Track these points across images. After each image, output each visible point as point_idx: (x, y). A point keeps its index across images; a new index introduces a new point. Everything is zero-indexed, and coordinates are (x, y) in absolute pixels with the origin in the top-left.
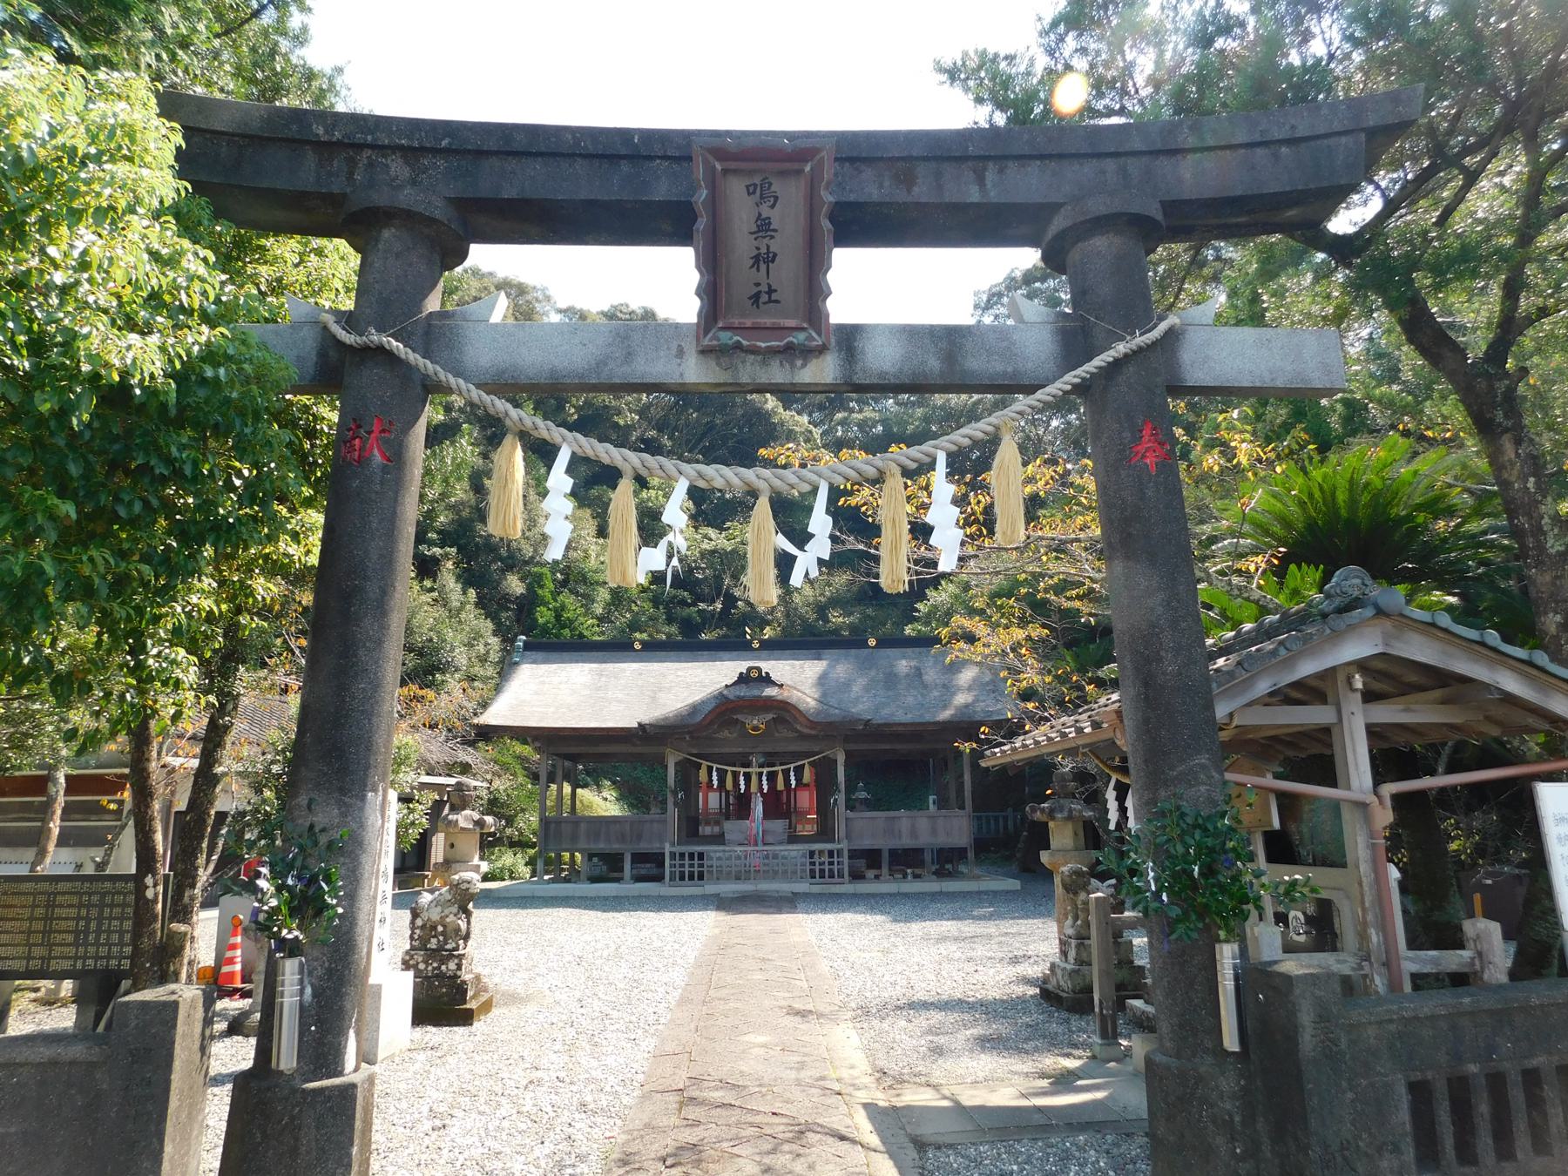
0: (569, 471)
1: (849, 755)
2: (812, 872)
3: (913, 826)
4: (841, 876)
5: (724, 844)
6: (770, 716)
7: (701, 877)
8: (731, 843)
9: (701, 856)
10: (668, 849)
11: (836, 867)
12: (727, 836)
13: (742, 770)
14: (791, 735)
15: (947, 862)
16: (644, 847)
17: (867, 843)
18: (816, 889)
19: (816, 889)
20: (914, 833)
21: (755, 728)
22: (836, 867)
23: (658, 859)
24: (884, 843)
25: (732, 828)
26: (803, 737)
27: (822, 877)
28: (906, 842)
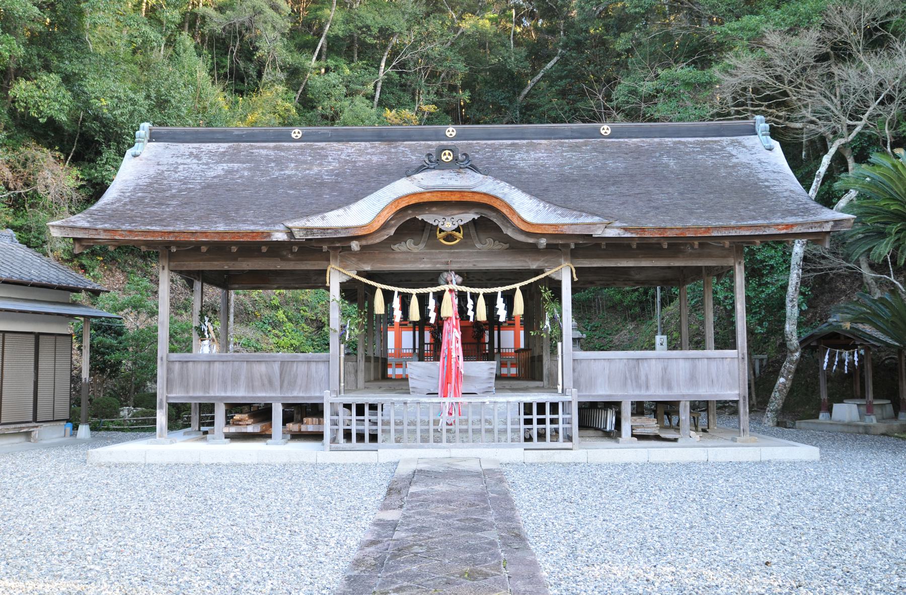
0: (434, 298)
3: (665, 369)
4: (569, 438)
5: (407, 392)
6: (470, 216)
7: (374, 438)
8: (416, 391)
9: (373, 407)
10: (329, 399)
11: (548, 426)
12: (411, 383)
13: (431, 290)
14: (498, 246)
15: (710, 414)
16: (299, 395)
20: (666, 382)
21: (450, 237)
22: (560, 426)
23: (316, 410)
24: (682, 391)
25: (416, 370)
26: (516, 248)
28: (656, 393)
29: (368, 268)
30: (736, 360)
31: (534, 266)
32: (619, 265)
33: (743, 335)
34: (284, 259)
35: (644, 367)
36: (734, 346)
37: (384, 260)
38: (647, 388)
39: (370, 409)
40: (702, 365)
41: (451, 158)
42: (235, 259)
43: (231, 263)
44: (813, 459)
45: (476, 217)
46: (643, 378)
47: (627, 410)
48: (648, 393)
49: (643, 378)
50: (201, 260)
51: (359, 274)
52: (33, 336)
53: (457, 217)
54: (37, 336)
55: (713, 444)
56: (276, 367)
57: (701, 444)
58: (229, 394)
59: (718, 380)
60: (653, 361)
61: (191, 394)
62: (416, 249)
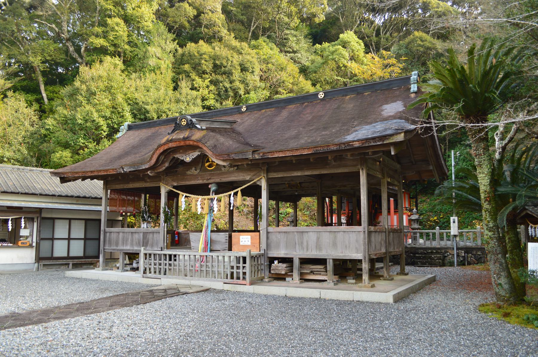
1: (268, 180)
2: (232, 273)
3: (318, 239)
17: (282, 253)
18: (227, 287)
19: (227, 287)
20: (318, 247)
24: (297, 254)
27: (238, 278)
29: (175, 184)
30: (362, 234)
31: (248, 178)
32: (293, 175)
33: (364, 215)
34: (146, 182)
35: (305, 236)
36: (359, 224)
37: (183, 180)
38: (307, 250)
39: (453, 262)
40: (340, 236)
41: (185, 123)
42: (128, 183)
43: (127, 185)
44: (388, 302)
45: (199, 153)
46: (305, 244)
47: (296, 263)
48: (308, 253)
49: (305, 244)
50: (117, 184)
51: (174, 187)
52: (83, 222)
53: (191, 155)
54: (70, 219)
55: (279, 285)
56: (141, 235)
57: (336, 287)
58: (125, 248)
59: (349, 246)
60: (311, 233)
61: (112, 248)
62: (196, 172)
